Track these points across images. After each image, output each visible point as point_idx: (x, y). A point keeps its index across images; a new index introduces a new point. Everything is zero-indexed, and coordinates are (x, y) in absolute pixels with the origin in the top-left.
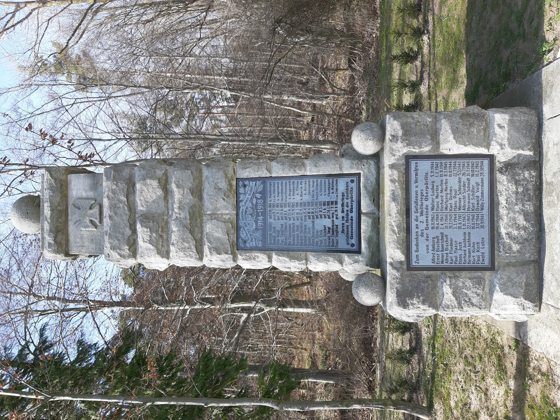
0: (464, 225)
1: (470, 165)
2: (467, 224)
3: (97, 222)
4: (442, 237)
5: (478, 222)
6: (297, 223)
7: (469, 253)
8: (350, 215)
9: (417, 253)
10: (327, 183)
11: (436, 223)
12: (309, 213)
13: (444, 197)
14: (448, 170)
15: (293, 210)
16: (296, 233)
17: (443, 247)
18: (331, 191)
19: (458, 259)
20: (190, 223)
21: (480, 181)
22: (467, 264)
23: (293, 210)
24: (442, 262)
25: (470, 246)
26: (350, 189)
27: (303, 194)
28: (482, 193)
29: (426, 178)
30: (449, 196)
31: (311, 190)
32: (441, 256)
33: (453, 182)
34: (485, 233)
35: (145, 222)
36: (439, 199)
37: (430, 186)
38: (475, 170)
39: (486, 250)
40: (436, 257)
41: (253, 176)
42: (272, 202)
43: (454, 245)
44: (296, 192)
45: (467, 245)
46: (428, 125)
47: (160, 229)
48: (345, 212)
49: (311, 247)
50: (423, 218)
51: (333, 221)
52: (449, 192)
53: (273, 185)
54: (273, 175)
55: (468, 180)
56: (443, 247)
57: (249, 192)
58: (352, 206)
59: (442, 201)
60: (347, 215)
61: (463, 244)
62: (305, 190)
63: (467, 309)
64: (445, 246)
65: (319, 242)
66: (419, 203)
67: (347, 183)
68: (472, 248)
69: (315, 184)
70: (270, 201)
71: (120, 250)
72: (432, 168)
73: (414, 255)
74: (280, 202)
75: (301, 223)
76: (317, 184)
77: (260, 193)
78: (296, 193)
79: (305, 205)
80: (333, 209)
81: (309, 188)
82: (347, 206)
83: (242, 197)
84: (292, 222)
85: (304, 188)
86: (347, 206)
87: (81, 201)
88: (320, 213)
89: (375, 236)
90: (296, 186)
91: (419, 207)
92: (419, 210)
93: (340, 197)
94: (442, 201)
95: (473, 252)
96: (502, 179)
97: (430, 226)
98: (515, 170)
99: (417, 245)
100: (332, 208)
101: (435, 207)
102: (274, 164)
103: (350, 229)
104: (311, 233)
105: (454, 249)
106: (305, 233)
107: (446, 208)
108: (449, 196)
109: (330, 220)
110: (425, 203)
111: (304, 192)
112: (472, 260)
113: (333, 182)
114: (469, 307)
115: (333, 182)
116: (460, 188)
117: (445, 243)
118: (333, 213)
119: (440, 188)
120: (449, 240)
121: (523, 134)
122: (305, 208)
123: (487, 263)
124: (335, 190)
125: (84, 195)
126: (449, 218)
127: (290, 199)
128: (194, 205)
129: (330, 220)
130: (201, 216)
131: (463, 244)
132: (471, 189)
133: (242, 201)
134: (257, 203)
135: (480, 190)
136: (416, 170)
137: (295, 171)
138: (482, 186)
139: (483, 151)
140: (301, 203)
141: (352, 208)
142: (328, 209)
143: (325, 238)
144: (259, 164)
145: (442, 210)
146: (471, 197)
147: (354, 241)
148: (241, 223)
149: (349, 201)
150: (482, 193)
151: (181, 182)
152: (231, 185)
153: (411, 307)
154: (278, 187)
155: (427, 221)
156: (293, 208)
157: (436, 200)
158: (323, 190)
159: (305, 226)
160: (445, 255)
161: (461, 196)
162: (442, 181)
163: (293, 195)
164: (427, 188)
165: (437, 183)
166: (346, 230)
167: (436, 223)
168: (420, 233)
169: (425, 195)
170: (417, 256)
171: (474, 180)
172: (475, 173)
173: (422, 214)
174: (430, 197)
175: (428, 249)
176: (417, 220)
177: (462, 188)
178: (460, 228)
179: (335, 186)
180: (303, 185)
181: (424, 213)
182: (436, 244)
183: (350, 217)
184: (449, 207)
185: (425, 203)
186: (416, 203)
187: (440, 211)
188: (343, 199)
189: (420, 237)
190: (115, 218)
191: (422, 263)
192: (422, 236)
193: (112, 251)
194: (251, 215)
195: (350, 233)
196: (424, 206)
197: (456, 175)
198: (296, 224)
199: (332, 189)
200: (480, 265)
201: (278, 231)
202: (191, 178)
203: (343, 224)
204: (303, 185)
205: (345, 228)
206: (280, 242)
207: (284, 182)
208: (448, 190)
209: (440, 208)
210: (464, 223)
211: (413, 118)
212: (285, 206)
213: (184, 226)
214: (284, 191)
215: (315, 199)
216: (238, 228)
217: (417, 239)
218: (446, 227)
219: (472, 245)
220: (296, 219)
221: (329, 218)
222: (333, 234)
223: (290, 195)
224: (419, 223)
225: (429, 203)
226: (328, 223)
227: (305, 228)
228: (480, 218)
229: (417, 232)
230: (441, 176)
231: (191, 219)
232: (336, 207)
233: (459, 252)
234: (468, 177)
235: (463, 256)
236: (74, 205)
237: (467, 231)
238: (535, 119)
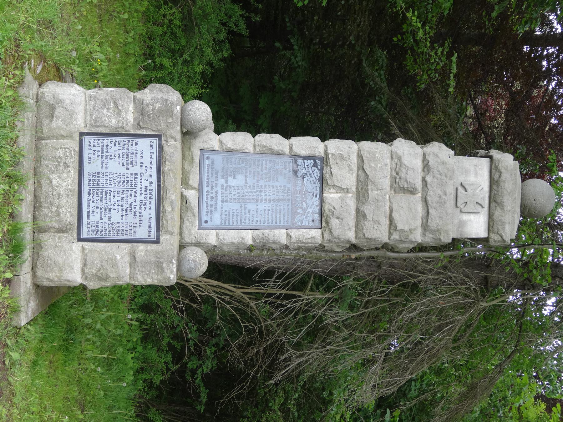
1: (99, 232)
2: (104, 176)
3: (461, 190)
4: (127, 166)
5: (94, 178)
6: (262, 182)
7: (103, 149)
9: (152, 151)
10: (231, 221)
11: (133, 179)
12: (250, 192)
13: (125, 202)
14: (120, 228)
15: (266, 195)
17: (127, 156)
18: (227, 213)
19: (113, 144)
20: (367, 186)
21: (91, 217)
22: (105, 139)
23: (266, 195)
24: (128, 141)
25: (102, 156)
26: (209, 214)
27: (255, 211)
28: (89, 206)
29: (141, 222)
30: (120, 204)
31: (247, 215)
32: (130, 148)
33: (116, 217)
34: (87, 168)
35: (412, 188)
38: (95, 228)
40: (134, 146)
41: (305, 231)
43: (117, 157)
44: (262, 212)
45: (104, 158)
46: (139, 271)
47: (397, 180)
48: (214, 191)
49: (249, 157)
50: (145, 184)
51: (227, 183)
53: (285, 221)
54: (285, 231)
56: (127, 156)
57: (309, 215)
58: (207, 198)
59: (127, 200)
60: (212, 189)
62: (253, 215)
63: (107, 97)
64: (125, 157)
65: (241, 162)
66: (148, 198)
67: (211, 221)
69: (243, 220)
70: (288, 205)
71: (437, 162)
72: (135, 231)
73: (155, 150)
75: (258, 182)
76: (241, 220)
77: (298, 213)
78: (262, 212)
79: (254, 200)
80: (226, 195)
81: (249, 217)
82: (212, 197)
84: (267, 183)
85: (255, 216)
86: (212, 197)
87: (475, 211)
88: (239, 191)
89: (186, 167)
90: (262, 219)
91: (148, 195)
92: (148, 191)
93: (219, 207)
94: (127, 200)
95: (99, 151)
96: (68, 215)
97: (139, 176)
98: (59, 226)
100: (227, 196)
101: (133, 193)
102: (284, 242)
104: (248, 172)
105: (117, 154)
107: (123, 192)
108: (120, 204)
109: (229, 184)
110: (143, 198)
111: (254, 213)
112: (100, 143)
113: (225, 222)
114: (105, 99)
115: (225, 222)
116: (110, 211)
117: (125, 160)
118: (226, 191)
119: (128, 212)
120: (121, 163)
121: (51, 259)
122: (269, 197)
123: (86, 139)
124: (224, 214)
125: (472, 217)
126: (121, 183)
127: (269, 207)
128: (363, 203)
129: (229, 184)
130: (358, 191)
132: (99, 210)
133: (317, 206)
134: (302, 203)
135: (91, 208)
136: (150, 230)
137: (263, 234)
138: (89, 212)
140: (258, 201)
142: (231, 195)
143: (235, 166)
144: (297, 243)
146: (99, 202)
147: (207, 162)
148: (318, 184)
149: (210, 203)
150: (89, 206)
151: (375, 226)
152: (327, 222)
154: (280, 219)
155: (141, 181)
156: (266, 197)
157: (132, 200)
158: (235, 214)
159: (254, 179)
160: (125, 149)
161: (109, 203)
162: (126, 219)
163: (265, 210)
164: (140, 212)
165: (130, 217)
166: (214, 174)
167: (133, 179)
168: (149, 169)
169: (142, 206)
170: (152, 148)
171: (96, 218)
172: (95, 225)
173: (146, 188)
174: (138, 203)
175: (142, 154)
176: (151, 182)
177: (107, 211)
178: (111, 174)
179: (224, 218)
180: (254, 220)
182: (134, 159)
185: (143, 198)
186: (151, 199)
187: (129, 190)
188: (216, 205)
189: (149, 166)
190: (440, 192)
191: (147, 141)
192: (146, 168)
193: (446, 160)
195: (210, 170)
196: (143, 195)
197: (113, 223)
198: (263, 181)
199: (226, 215)
200: (93, 138)
201: (281, 174)
202: (365, 231)
203: (216, 180)
206: (279, 164)
208: (120, 210)
209: (129, 193)
210: (107, 178)
211: (152, 278)
213: (373, 183)
215: (243, 206)
216: (322, 179)
217: (151, 165)
218: (123, 174)
219: (100, 157)
220: (263, 187)
221: (230, 186)
223: (269, 210)
224: (150, 180)
225: (139, 198)
226: (232, 182)
227: (254, 177)
228: (92, 182)
229: (151, 171)
230: (127, 223)
231: (367, 190)
232: (223, 196)
233: (112, 151)
234: (101, 221)
235: (109, 147)
236: (483, 207)
238: (40, 272)
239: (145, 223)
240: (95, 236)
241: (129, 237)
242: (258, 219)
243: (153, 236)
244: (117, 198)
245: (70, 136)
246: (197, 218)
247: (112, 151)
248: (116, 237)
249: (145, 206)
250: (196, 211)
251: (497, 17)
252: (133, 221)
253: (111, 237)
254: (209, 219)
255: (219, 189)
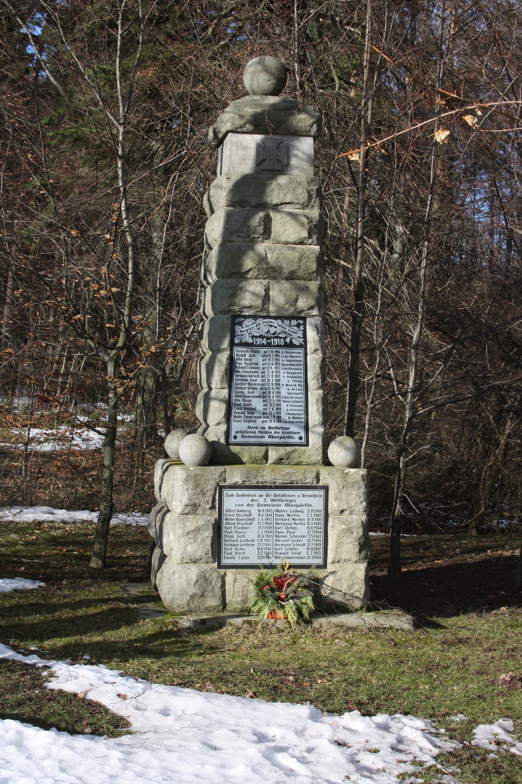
0: (261, 540)
8: (266, 436)
13: (287, 522)
16: (249, 378)
18: (291, 416)
25: (242, 545)
28: (291, 558)
30: (289, 526)
31: (293, 396)
33: (302, 530)
36: (286, 517)
37: (299, 509)
39: (237, 561)
42: (281, 354)
44: (290, 380)
50: (269, 502)
52: (293, 526)
55: (304, 544)
60: (266, 432)
61: (243, 539)
66: (283, 498)
68: (239, 547)
72: (316, 510)
73: (234, 492)
74: (281, 362)
82: (275, 433)
83: (287, 322)
86: (275, 433)
92: (276, 498)
97: (261, 508)
99: (243, 495)
103: (251, 435)
106: (249, 388)
107: (277, 524)
108: (289, 526)
111: (290, 388)
119: (297, 518)
124: (292, 420)
131: (243, 539)
134: (280, 338)
135: (294, 556)
136: (314, 496)
138: (298, 558)
139: (330, 560)
141: (273, 437)
145: (276, 519)
146: (288, 547)
147: (239, 439)
149: (281, 435)
150: (291, 558)
153: (186, 487)
155: (265, 505)
158: (292, 408)
168: (254, 498)
170: (233, 495)
171: (303, 550)
173: (273, 500)
174: (288, 508)
176: (267, 495)
181: (274, 503)
183: (264, 435)
184: (278, 526)
185: (283, 504)
186: (284, 495)
188: (283, 428)
189: (251, 498)
192: (252, 500)
194: (269, 331)
197: (309, 533)
203: (257, 428)
204: (297, 387)
205: (253, 430)
207: (302, 367)
212: (277, 368)
214: (292, 367)
217: (249, 495)
218: (260, 523)
222: (247, 417)
225: (285, 508)
230: (308, 519)
233: (235, 536)
237: (256, 543)
239: (308, 500)
240: (322, 550)
241: (322, 517)
242: (297, 384)
243: (322, 493)
244: (284, 530)
245: (223, 578)
246: (297, 448)
247: (235, 536)
248: (322, 530)
249: (291, 501)
250: (289, 449)
251: (457, 329)
252: (306, 512)
253: (322, 535)
254: (298, 435)
255: (266, 425)
